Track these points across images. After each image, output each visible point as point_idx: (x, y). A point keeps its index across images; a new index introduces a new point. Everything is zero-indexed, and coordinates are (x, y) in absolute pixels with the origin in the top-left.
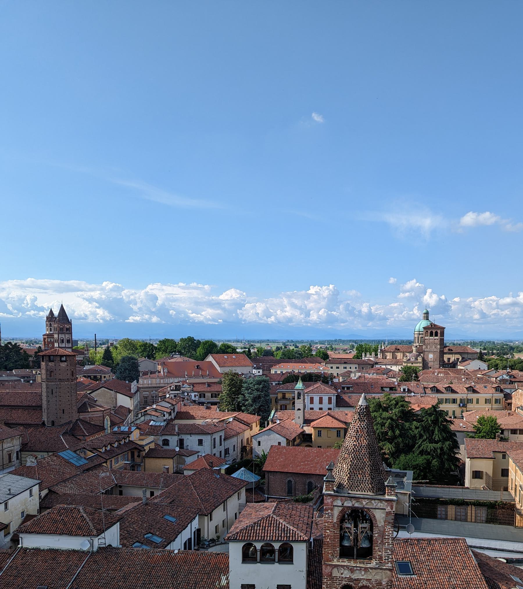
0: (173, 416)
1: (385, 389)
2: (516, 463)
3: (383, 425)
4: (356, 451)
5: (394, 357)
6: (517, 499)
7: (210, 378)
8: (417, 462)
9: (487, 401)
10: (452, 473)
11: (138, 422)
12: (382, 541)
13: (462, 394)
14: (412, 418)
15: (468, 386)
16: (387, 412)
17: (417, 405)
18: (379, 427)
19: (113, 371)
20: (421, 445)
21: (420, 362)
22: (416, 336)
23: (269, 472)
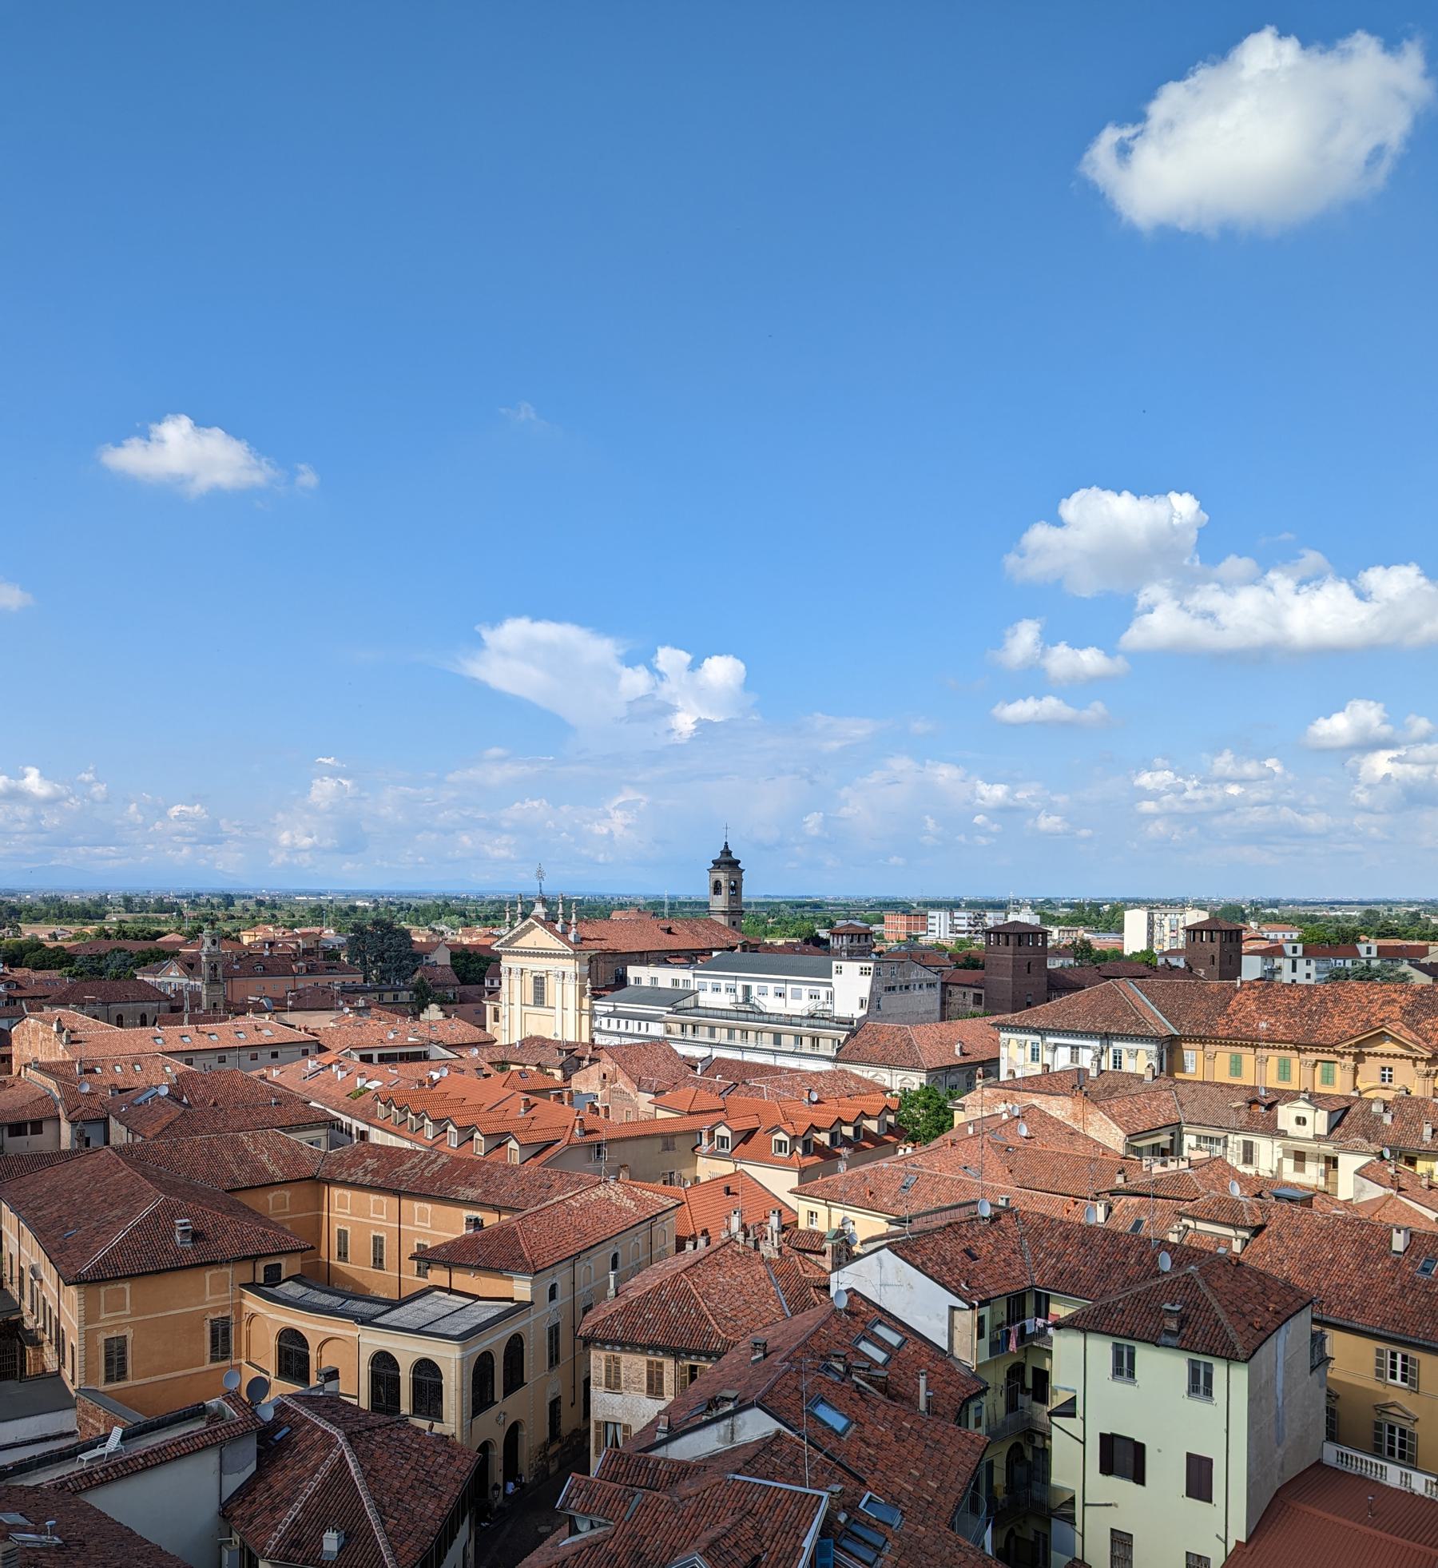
2: (17, 1213)
6: (26, 1305)
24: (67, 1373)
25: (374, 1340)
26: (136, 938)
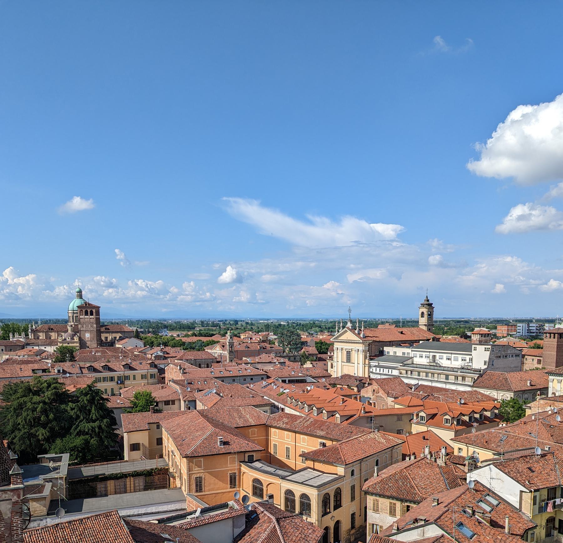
2: (167, 432)
3: (34, 410)
5: (48, 337)
6: (170, 464)
8: (75, 444)
9: (143, 377)
12: (10, 534)
13: (121, 372)
14: (67, 400)
15: (124, 363)
16: (39, 395)
17: (73, 386)
18: (30, 412)
20: (78, 426)
21: (76, 342)
22: (70, 315)
25: (286, 485)
26: (205, 336)
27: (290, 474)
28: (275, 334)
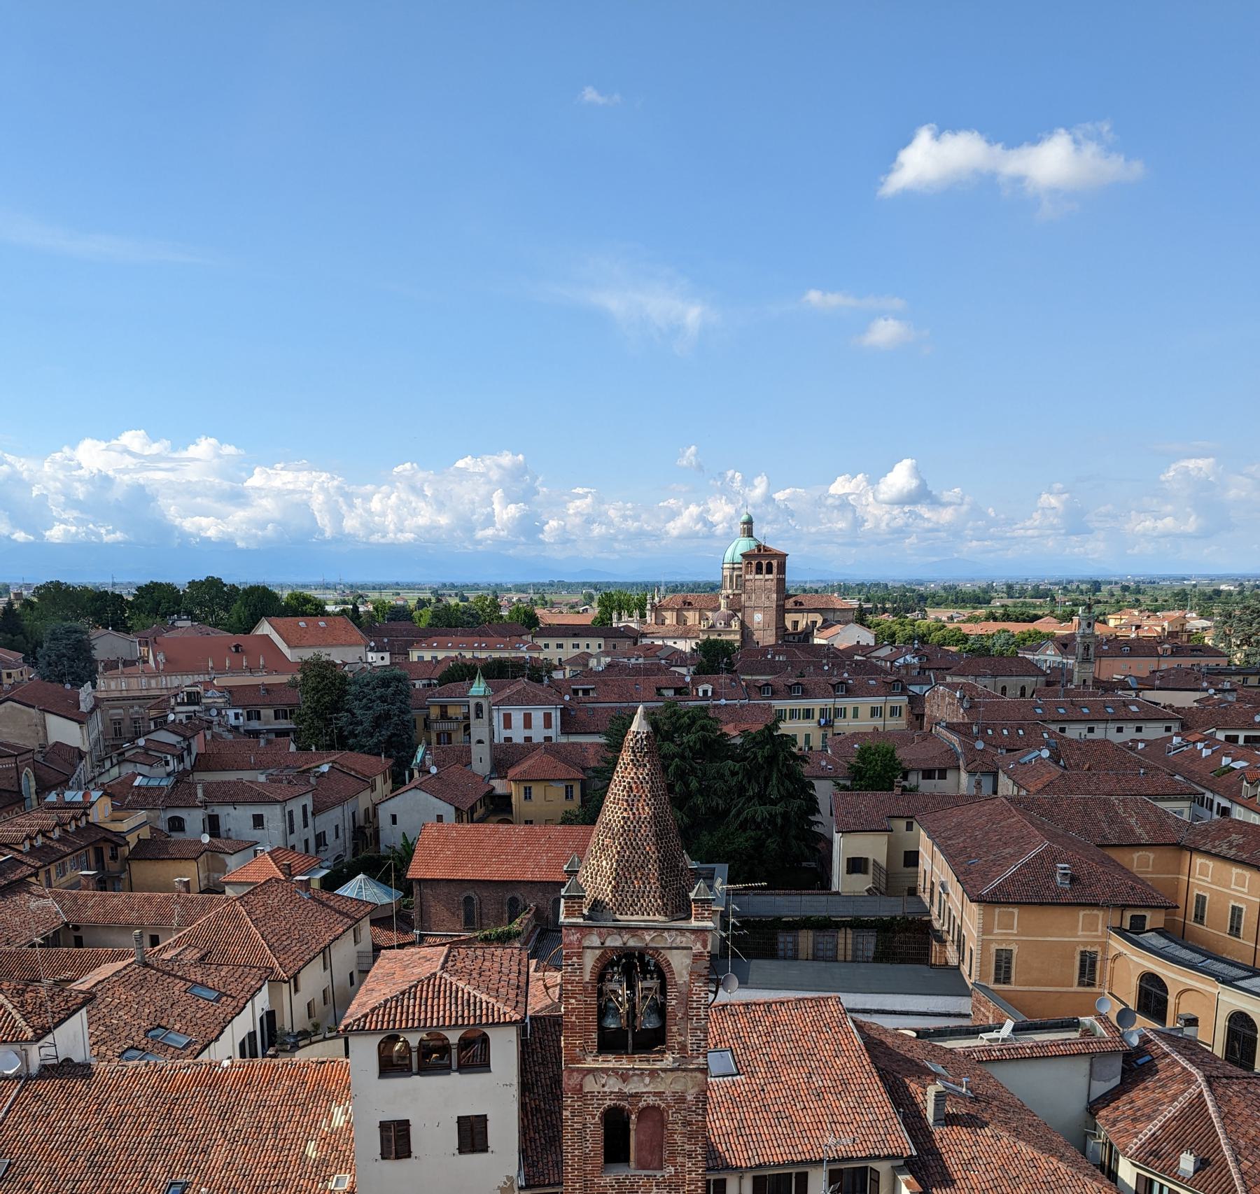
0: (188, 763)
1: (665, 692)
2: (933, 839)
4: (629, 829)
5: (681, 620)
6: (935, 910)
7: (269, 673)
10: (804, 864)
11: (105, 779)
12: (686, 1014)
15: (835, 680)
19: (31, 658)
22: (727, 573)
23: (420, 881)
24: (965, 969)
25: (1233, 1000)
26: (1017, 620)
27: (1246, 974)
28: (1201, 616)
